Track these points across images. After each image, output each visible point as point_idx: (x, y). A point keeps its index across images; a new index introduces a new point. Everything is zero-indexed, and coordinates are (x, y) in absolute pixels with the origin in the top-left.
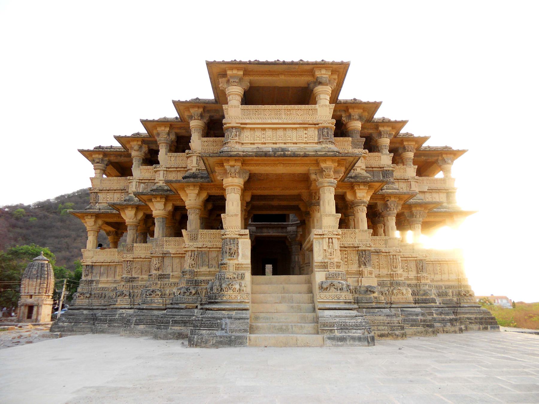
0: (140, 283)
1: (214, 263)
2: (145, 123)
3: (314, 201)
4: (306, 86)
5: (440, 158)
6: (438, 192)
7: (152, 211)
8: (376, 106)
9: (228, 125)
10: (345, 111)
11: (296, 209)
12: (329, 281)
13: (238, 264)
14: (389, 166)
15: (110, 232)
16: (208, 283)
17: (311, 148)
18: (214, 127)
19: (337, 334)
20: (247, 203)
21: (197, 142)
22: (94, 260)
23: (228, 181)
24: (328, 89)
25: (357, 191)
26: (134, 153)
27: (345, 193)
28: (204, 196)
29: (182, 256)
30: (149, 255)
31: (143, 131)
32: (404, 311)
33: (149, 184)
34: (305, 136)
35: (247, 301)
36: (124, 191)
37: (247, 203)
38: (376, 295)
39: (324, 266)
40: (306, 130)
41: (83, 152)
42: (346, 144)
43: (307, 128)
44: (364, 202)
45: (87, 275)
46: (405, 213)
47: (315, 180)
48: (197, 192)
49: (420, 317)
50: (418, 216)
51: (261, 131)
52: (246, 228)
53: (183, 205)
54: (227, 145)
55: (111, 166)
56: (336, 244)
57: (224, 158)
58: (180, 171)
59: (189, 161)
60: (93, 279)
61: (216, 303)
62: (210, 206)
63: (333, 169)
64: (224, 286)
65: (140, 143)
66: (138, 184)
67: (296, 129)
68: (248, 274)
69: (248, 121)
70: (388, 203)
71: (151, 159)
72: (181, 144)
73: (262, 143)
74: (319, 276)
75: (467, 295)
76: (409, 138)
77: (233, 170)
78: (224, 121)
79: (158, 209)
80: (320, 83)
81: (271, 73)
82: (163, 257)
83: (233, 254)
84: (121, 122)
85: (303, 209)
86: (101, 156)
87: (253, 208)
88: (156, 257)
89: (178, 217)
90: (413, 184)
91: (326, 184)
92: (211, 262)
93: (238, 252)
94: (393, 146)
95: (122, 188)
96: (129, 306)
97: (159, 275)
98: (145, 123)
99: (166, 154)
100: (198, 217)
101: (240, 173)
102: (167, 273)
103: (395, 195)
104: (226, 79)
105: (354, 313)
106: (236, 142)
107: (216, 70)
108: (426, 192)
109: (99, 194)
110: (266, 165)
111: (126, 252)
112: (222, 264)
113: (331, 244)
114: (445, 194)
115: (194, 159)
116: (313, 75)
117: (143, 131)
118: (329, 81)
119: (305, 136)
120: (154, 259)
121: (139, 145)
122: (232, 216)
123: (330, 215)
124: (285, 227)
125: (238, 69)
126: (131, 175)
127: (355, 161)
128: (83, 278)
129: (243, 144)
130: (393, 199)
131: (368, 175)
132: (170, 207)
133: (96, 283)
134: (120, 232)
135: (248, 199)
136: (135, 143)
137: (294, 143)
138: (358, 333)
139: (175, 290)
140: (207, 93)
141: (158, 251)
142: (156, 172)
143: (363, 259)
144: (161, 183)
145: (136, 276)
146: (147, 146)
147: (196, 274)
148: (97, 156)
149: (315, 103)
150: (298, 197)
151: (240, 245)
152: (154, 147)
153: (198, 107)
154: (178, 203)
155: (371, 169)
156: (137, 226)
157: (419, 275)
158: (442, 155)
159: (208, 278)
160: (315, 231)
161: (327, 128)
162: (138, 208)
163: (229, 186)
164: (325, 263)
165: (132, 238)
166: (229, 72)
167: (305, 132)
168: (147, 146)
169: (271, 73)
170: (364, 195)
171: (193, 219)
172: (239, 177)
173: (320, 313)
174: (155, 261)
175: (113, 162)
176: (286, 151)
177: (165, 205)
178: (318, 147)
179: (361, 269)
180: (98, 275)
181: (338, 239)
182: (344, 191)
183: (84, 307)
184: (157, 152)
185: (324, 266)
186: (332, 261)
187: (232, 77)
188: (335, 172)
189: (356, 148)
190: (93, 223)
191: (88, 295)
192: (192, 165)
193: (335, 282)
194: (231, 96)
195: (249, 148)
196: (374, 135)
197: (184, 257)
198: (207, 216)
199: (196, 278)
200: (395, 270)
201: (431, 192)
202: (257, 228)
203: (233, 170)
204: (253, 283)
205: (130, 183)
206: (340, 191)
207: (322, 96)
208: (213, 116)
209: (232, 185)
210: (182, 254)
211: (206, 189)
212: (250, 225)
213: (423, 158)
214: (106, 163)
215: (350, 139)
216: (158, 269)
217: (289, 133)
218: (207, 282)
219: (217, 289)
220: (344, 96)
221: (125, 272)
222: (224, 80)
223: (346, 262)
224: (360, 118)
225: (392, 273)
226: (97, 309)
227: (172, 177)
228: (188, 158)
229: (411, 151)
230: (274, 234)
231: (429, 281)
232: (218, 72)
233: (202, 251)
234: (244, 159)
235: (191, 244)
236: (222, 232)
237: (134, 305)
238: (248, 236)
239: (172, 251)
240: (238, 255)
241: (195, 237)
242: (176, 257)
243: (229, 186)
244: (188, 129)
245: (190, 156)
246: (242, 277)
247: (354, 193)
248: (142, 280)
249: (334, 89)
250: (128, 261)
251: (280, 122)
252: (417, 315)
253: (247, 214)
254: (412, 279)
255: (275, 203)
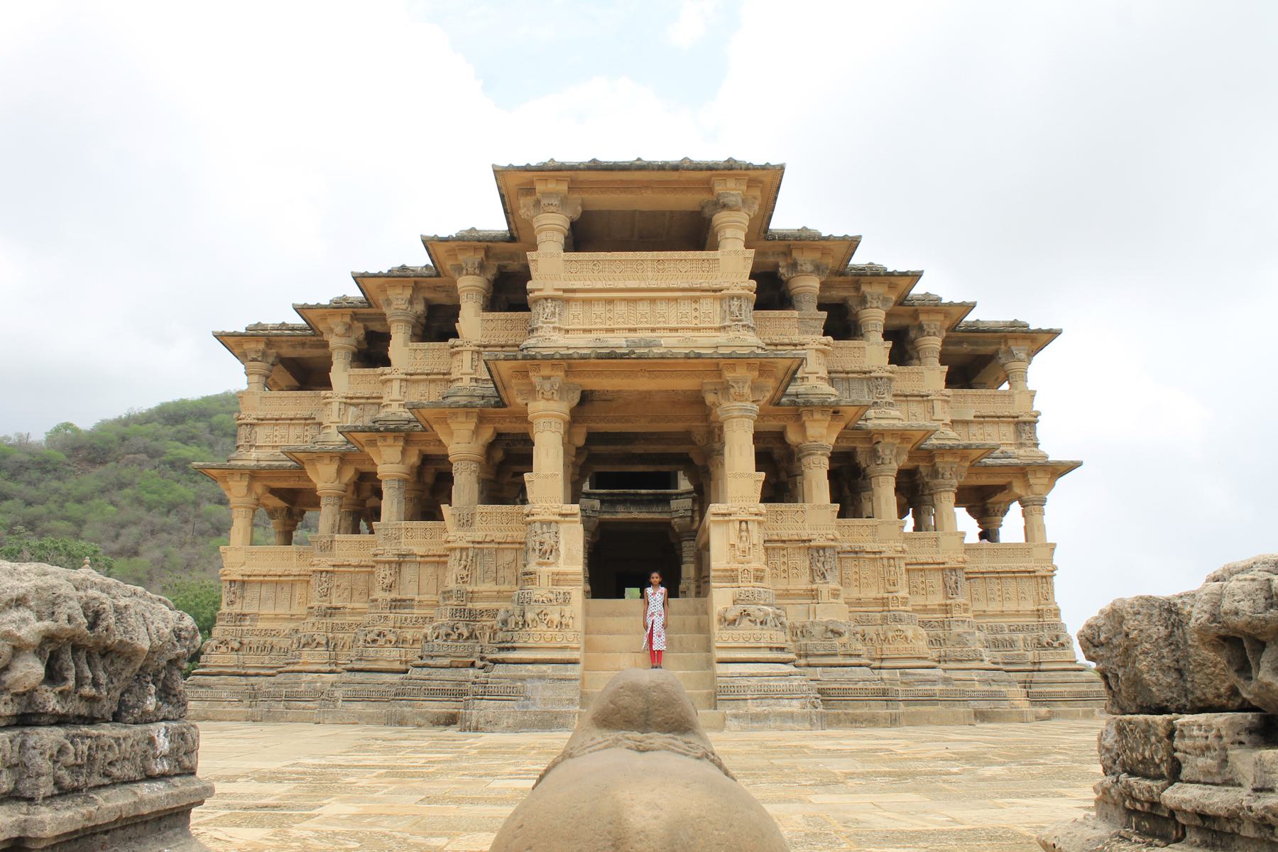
0: (349, 619)
1: (507, 573)
2: (360, 279)
3: (717, 446)
4: (698, 209)
5: (1003, 347)
6: (997, 423)
7: (374, 464)
8: (852, 244)
9: (537, 294)
10: (785, 254)
11: (685, 461)
12: (739, 608)
13: (558, 574)
14: (880, 368)
15: (276, 510)
16: (495, 616)
17: (705, 342)
18: (509, 291)
19: (752, 707)
20: (578, 449)
21: (473, 322)
22: (247, 570)
23: (537, 407)
24: (743, 218)
25: (807, 424)
26: (334, 341)
27: (785, 427)
28: (487, 434)
29: (440, 561)
30: (367, 560)
31: (355, 293)
32: (907, 674)
33: (368, 407)
34: (695, 314)
35: (574, 645)
36: (309, 421)
37: (578, 449)
38: (844, 639)
39: (731, 576)
40: (696, 302)
41: (222, 337)
42: (787, 323)
43: (699, 298)
44: (822, 447)
45: (232, 603)
46: (921, 469)
47: (714, 404)
48: (472, 426)
49: (939, 687)
50: (947, 475)
51: (605, 311)
52: (574, 501)
53: (441, 453)
54: (535, 334)
55: (280, 366)
56: (756, 536)
57: (530, 361)
58: (434, 381)
59: (455, 362)
60: (245, 611)
61: (514, 649)
62: (499, 455)
63: (749, 383)
64: (530, 616)
65: (348, 319)
66: (342, 407)
67: (676, 299)
68: (578, 592)
69: (577, 285)
70: (879, 448)
71: (372, 352)
72: (437, 324)
73: (607, 330)
74: (721, 598)
75: (1056, 644)
76: (933, 305)
77: (547, 386)
78: (529, 285)
79: (390, 464)
80: (725, 206)
81: (626, 187)
82: (400, 564)
83: (547, 553)
84: (307, 273)
85: (698, 461)
86: (261, 346)
87: (593, 459)
88: (385, 562)
89: (429, 479)
90: (938, 405)
91: (736, 413)
92: (501, 573)
93: (557, 550)
94: (896, 322)
95: (306, 414)
96: (328, 668)
97: (393, 600)
98: (360, 279)
99: (406, 345)
100: (474, 478)
101: (562, 391)
102: (409, 596)
103: (894, 433)
104: (534, 198)
105: (788, 668)
106: (554, 328)
107: (513, 181)
108: (972, 422)
109: (257, 429)
110: (613, 374)
111: (317, 552)
112: (526, 574)
113: (744, 534)
114: (1012, 428)
115: (467, 357)
116: (711, 191)
117: (355, 293)
118: (744, 201)
119: (695, 314)
120: (382, 567)
121: (345, 323)
122: (546, 477)
123: (741, 475)
124: (666, 500)
125: (558, 180)
126: (327, 385)
127: (794, 367)
128: (225, 609)
129: (567, 331)
130: (888, 440)
131: (832, 390)
132: (414, 459)
133: (252, 620)
134: (296, 509)
135: (580, 441)
136: (338, 320)
137: (671, 330)
138: (795, 706)
139: (428, 630)
140: (494, 221)
141: (389, 551)
142: (385, 382)
143: (820, 565)
144: (395, 408)
145: (339, 605)
146: (361, 325)
147: (472, 596)
148: (253, 345)
149: (715, 247)
150: (686, 437)
151: (561, 535)
152: (377, 327)
153: (475, 249)
154: (432, 450)
155: (844, 375)
156: (341, 498)
157: (949, 602)
158: (1006, 342)
159: (494, 605)
160: (713, 508)
161: (739, 298)
162: (343, 458)
163: (540, 416)
164: (732, 570)
165: (331, 522)
166: (540, 187)
167: (694, 306)
168: (361, 325)
169: (626, 187)
170: (820, 437)
171: (465, 484)
172: (561, 399)
173: (721, 669)
174: (383, 572)
175: (292, 360)
176: (656, 346)
177: (404, 452)
178: (722, 338)
179: (814, 587)
180: (256, 602)
181: (760, 523)
182: (783, 423)
183: (229, 670)
184: (386, 337)
185: (731, 576)
186: (746, 566)
187: (545, 194)
188: (755, 388)
189: (807, 332)
190: (245, 490)
191: (236, 645)
192: (464, 371)
193: (751, 609)
194: (543, 234)
195: (579, 342)
196: (852, 303)
197: (445, 563)
198: (492, 477)
199: (470, 606)
200: (891, 588)
201: (981, 423)
202: (602, 502)
203: (547, 386)
204: (587, 612)
205: (326, 404)
206: (772, 425)
207: (729, 233)
208: (505, 267)
209: (546, 416)
210: (440, 556)
211: (491, 421)
212: (588, 496)
213: (966, 348)
214: (271, 360)
215: (796, 313)
216: (390, 588)
217: (661, 308)
218: (494, 613)
219: (517, 623)
220: (782, 221)
221: (317, 595)
222: (529, 200)
223: (784, 571)
224: (818, 269)
225: (886, 595)
226: (257, 675)
227: (417, 394)
228: (453, 355)
229: (934, 334)
230: (642, 516)
231: (970, 614)
232: (517, 185)
233: (482, 549)
234: (569, 363)
235: (461, 534)
236: (526, 509)
237: (336, 664)
238: (578, 519)
239: (416, 550)
240: (558, 556)
241: (467, 517)
242: (427, 563)
243: (540, 416)
244: (452, 289)
245: (458, 353)
246: (566, 600)
247: (803, 428)
248: (354, 612)
249: (755, 216)
250: (321, 572)
251: (643, 285)
252: (934, 682)
253: (578, 471)
254: (934, 611)
255: (638, 449)
